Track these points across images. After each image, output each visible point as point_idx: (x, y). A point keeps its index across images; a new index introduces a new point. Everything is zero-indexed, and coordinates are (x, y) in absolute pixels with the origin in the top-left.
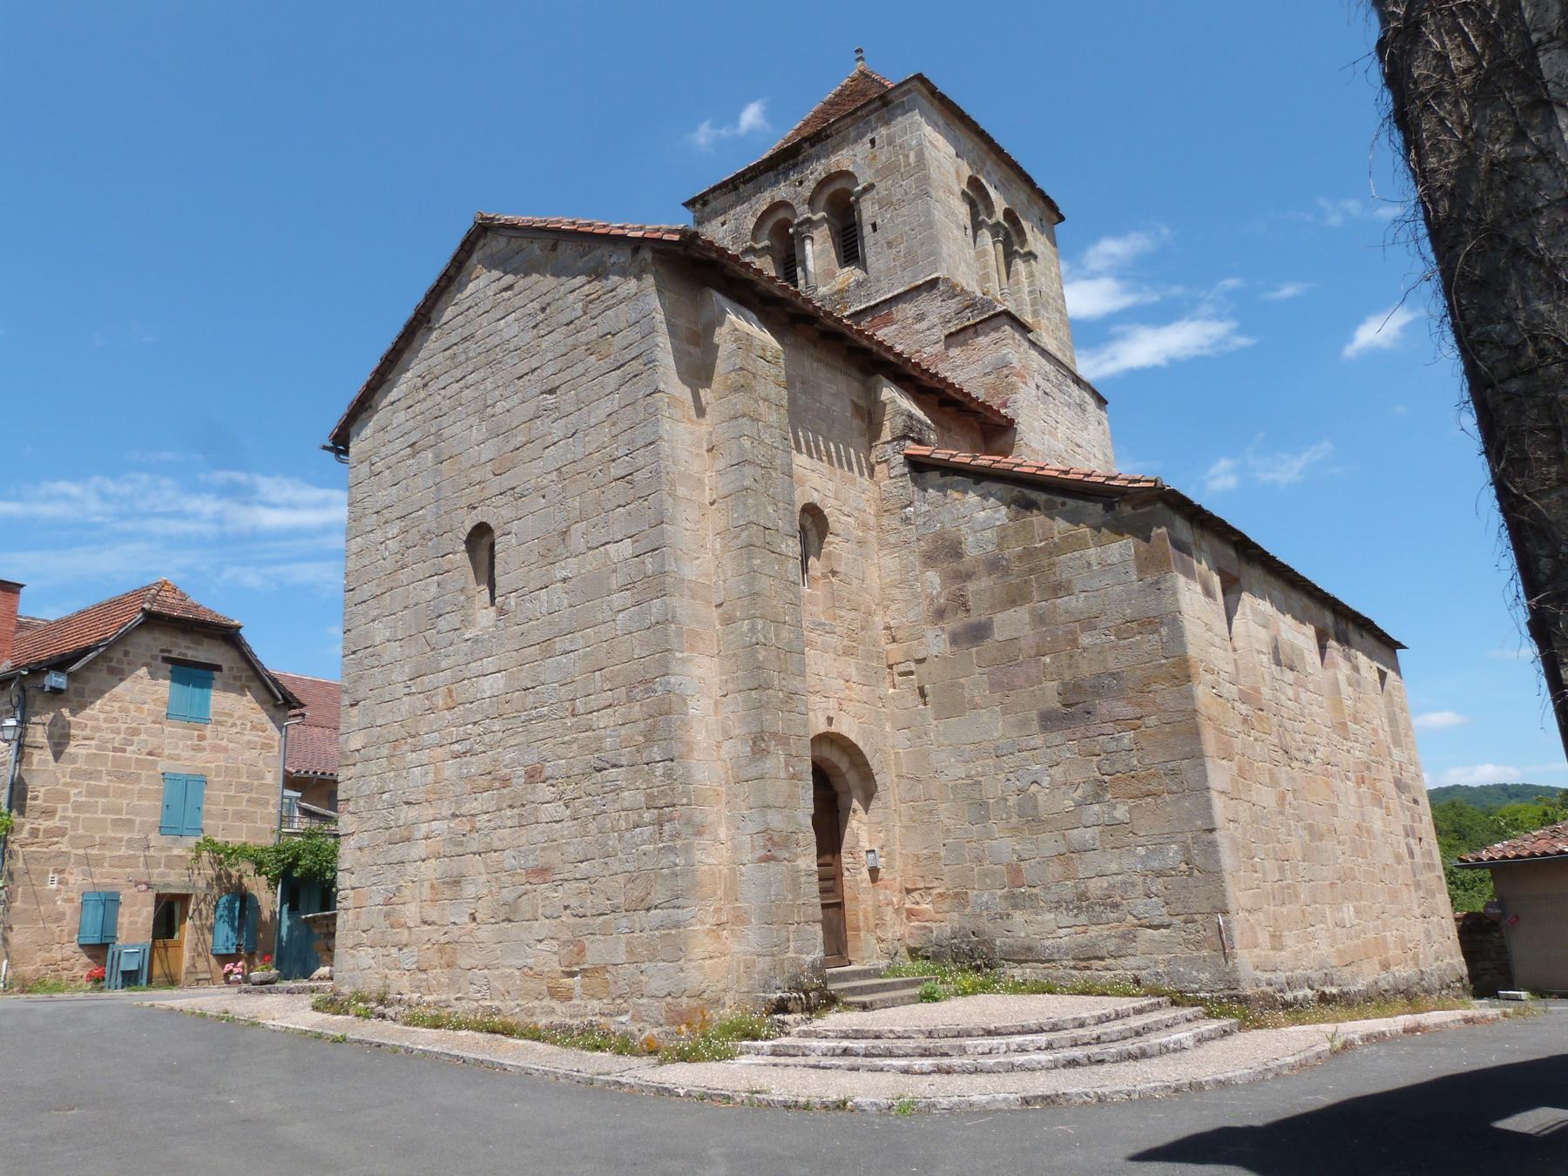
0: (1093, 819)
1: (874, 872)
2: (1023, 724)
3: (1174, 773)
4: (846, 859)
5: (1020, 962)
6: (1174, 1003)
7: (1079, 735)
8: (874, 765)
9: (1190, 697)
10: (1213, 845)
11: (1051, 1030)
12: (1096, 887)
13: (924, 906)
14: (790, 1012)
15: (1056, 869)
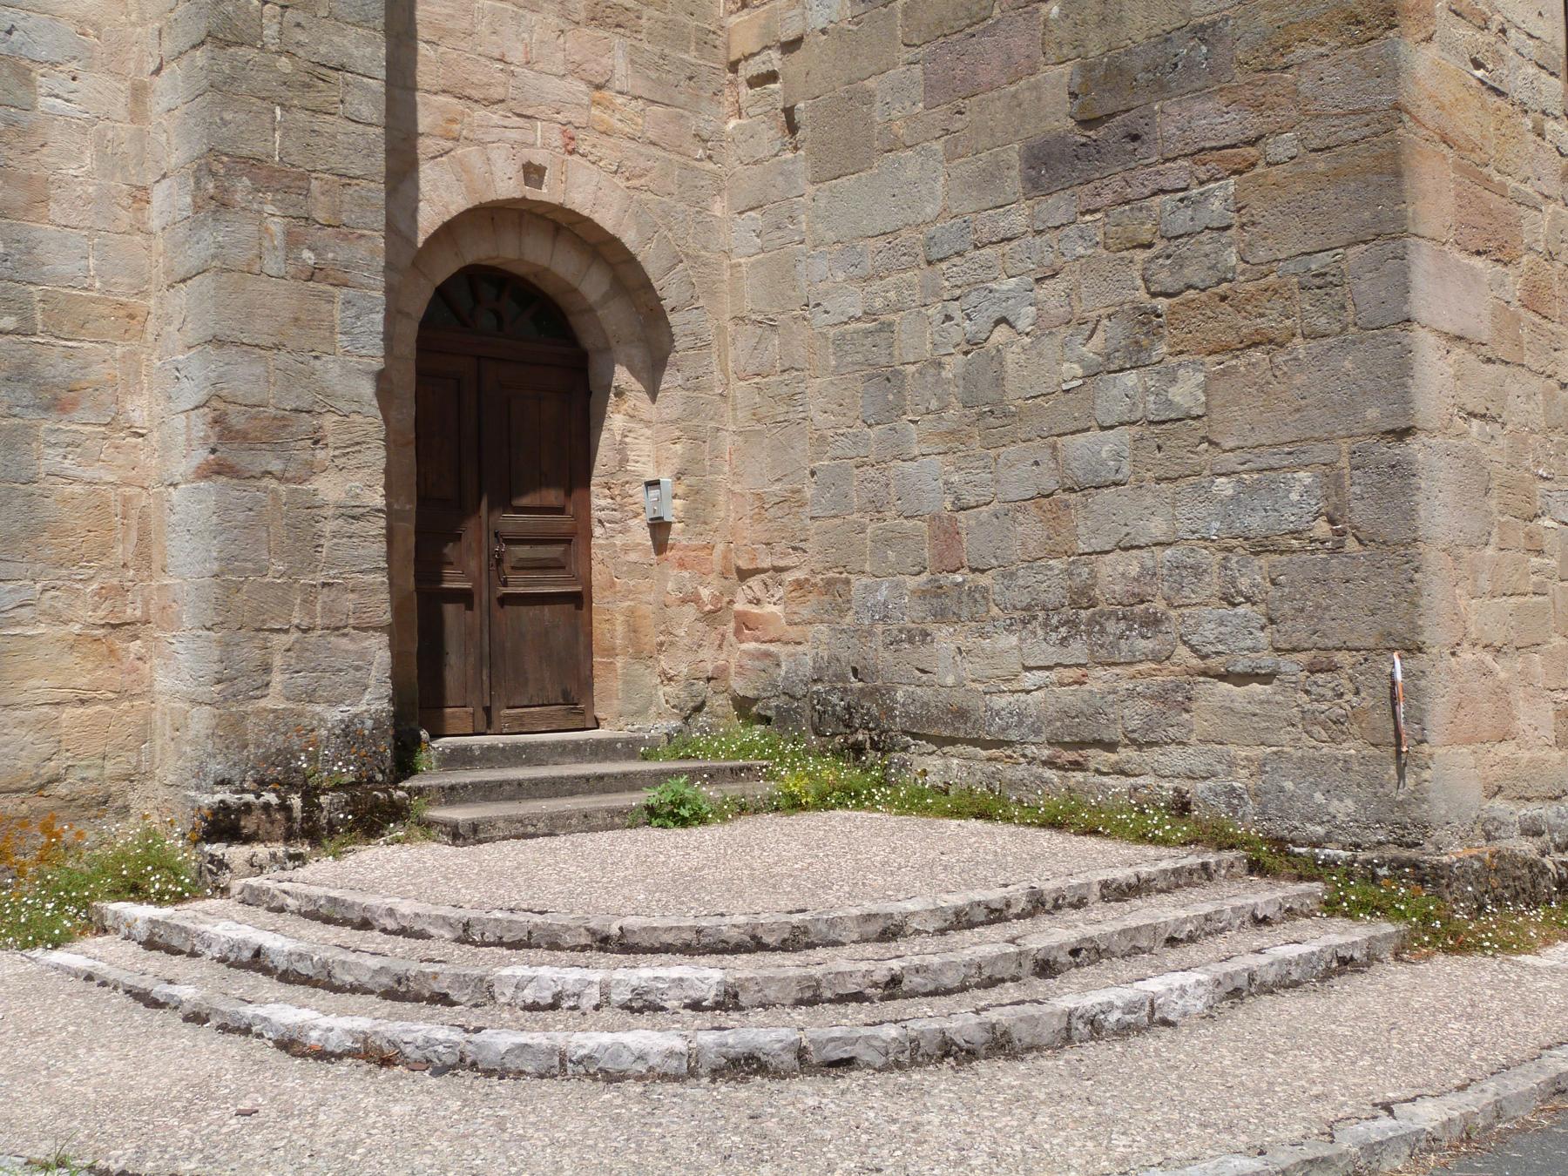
0: (1120, 410)
1: (659, 528)
2: (990, 178)
3: (1323, 282)
4: (599, 499)
5: (942, 742)
6: (1256, 867)
7: (1108, 197)
8: (670, 290)
9: (1392, 71)
10: (1402, 471)
11: (784, 947)
12: (1115, 574)
13: (769, 609)
14: (247, 840)
15: (1030, 530)
